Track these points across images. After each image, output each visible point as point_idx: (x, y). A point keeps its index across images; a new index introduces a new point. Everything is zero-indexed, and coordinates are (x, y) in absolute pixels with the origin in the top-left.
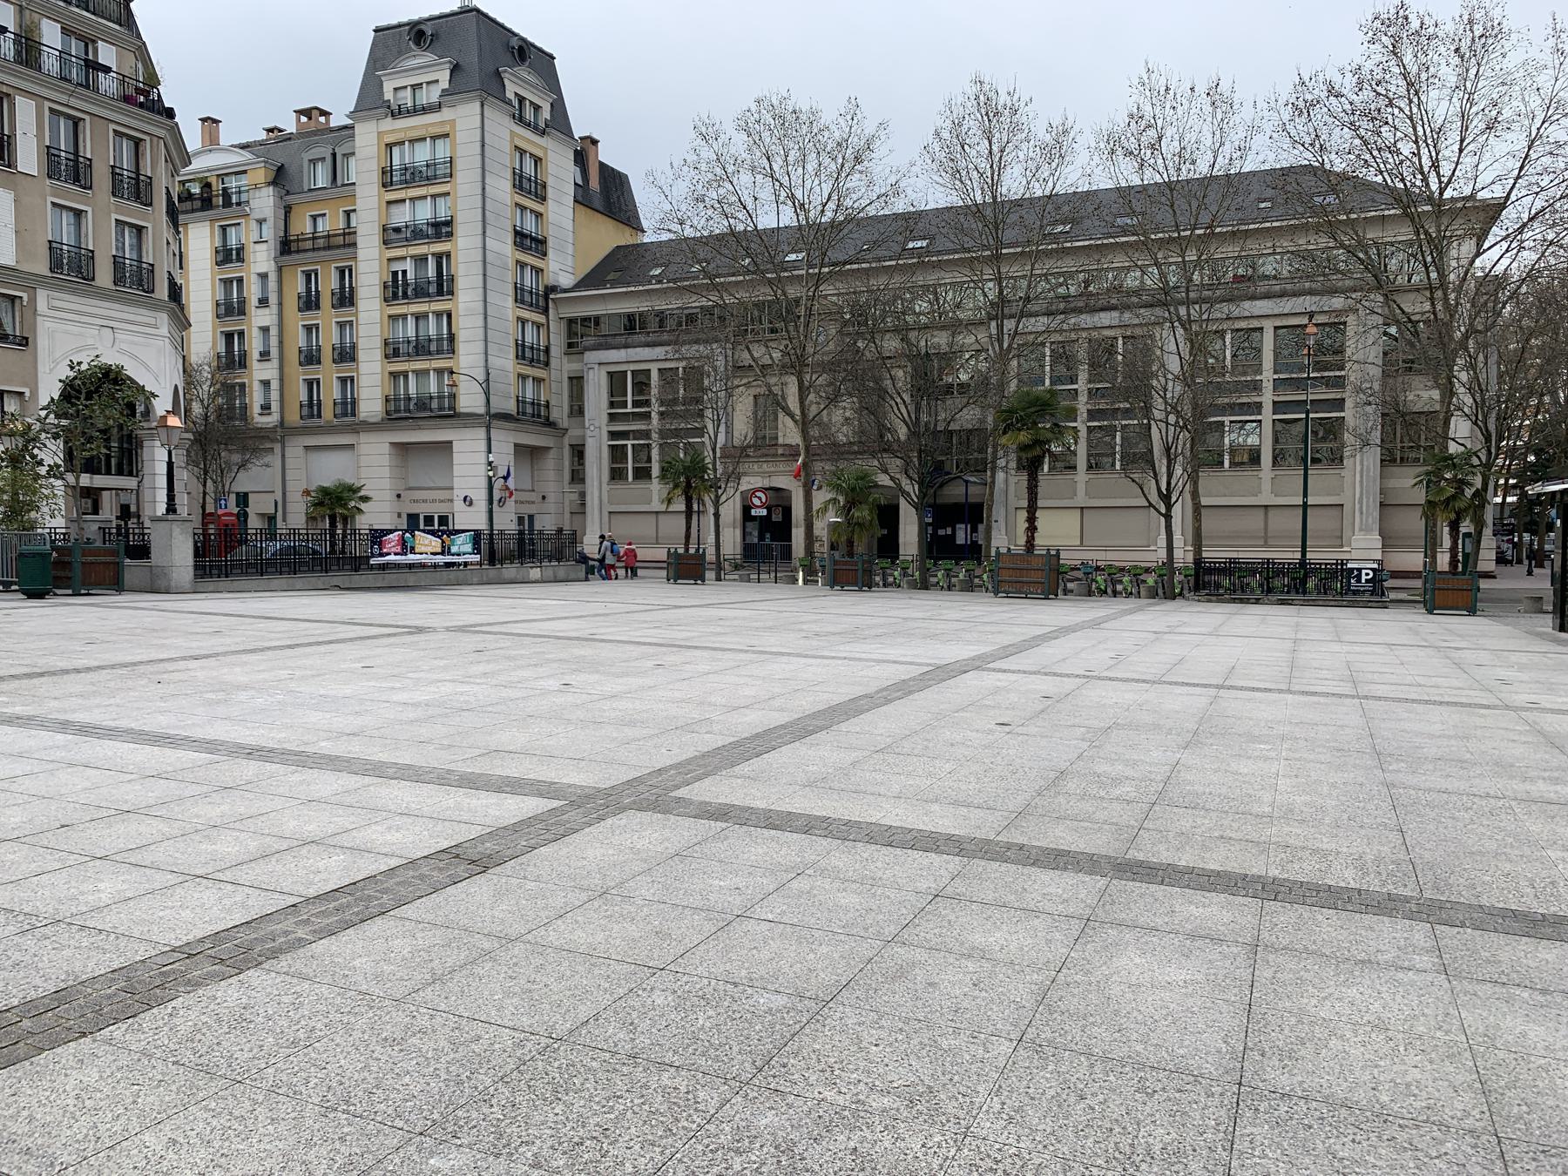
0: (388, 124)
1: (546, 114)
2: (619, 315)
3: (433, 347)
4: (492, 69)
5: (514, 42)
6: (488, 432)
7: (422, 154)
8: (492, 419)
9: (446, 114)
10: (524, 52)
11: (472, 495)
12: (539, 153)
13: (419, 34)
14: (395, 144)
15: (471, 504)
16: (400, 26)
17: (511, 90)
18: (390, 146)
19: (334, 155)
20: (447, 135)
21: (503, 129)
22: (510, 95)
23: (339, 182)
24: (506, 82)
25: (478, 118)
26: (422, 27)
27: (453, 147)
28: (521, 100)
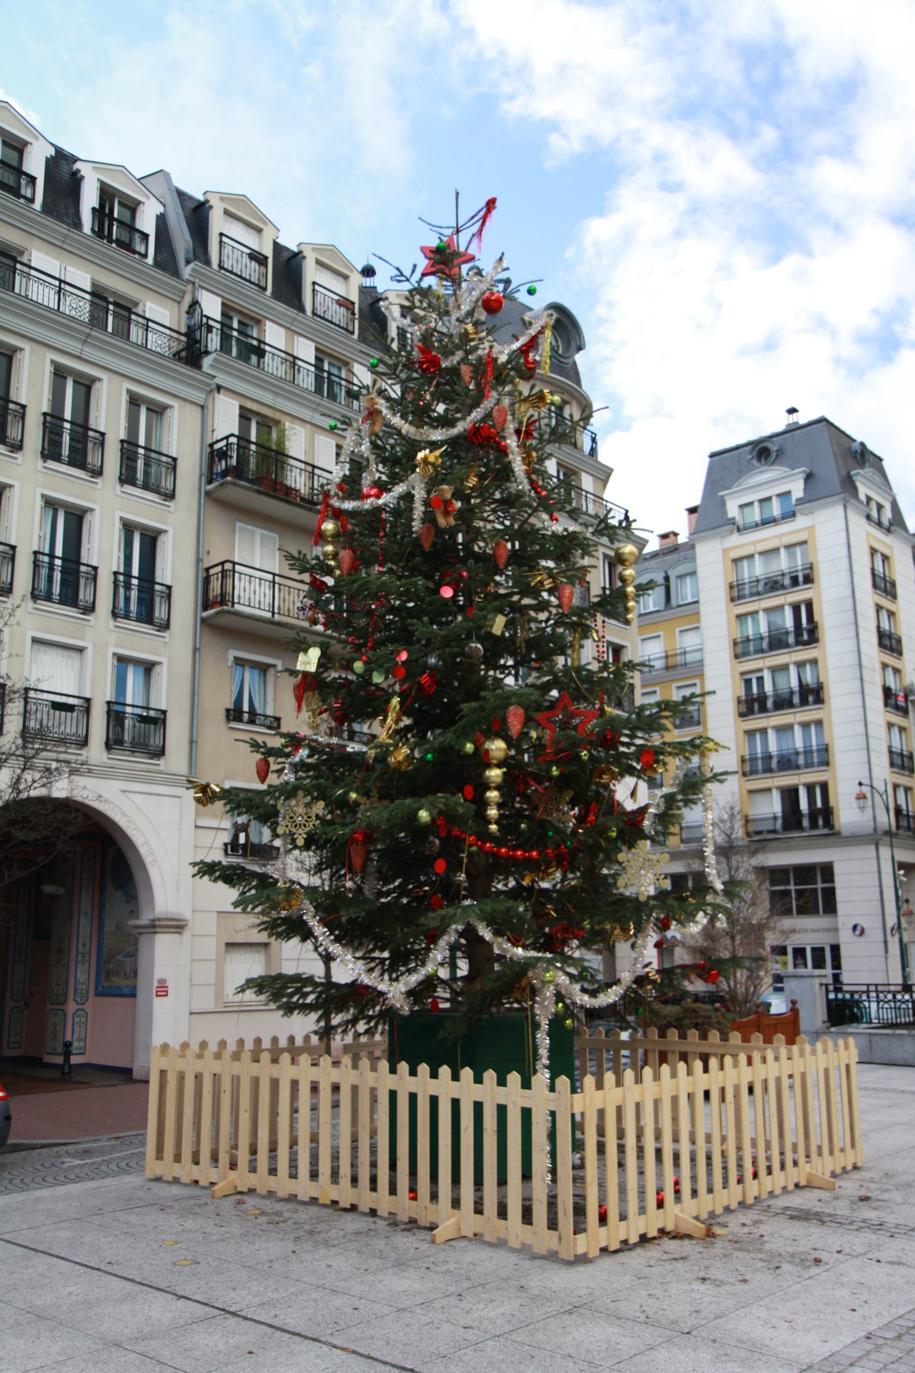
0: (735, 540)
1: (887, 514)
2: (149, 1062)
3: (801, 760)
4: (844, 473)
5: (855, 446)
6: (877, 849)
7: (783, 563)
8: (875, 838)
9: (801, 522)
10: (862, 456)
11: (862, 922)
12: (886, 552)
13: (763, 451)
14: (741, 559)
15: (862, 932)
16: (738, 448)
17: (863, 491)
18: (736, 561)
19: (667, 579)
20: (805, 542)
21: (864, 533)
22: (862, 497)
23: (674, 602)
24: (859, 485)
25: (843, 520)
26: (766, 444)
27: (696, 585)
28: (869, 499)
